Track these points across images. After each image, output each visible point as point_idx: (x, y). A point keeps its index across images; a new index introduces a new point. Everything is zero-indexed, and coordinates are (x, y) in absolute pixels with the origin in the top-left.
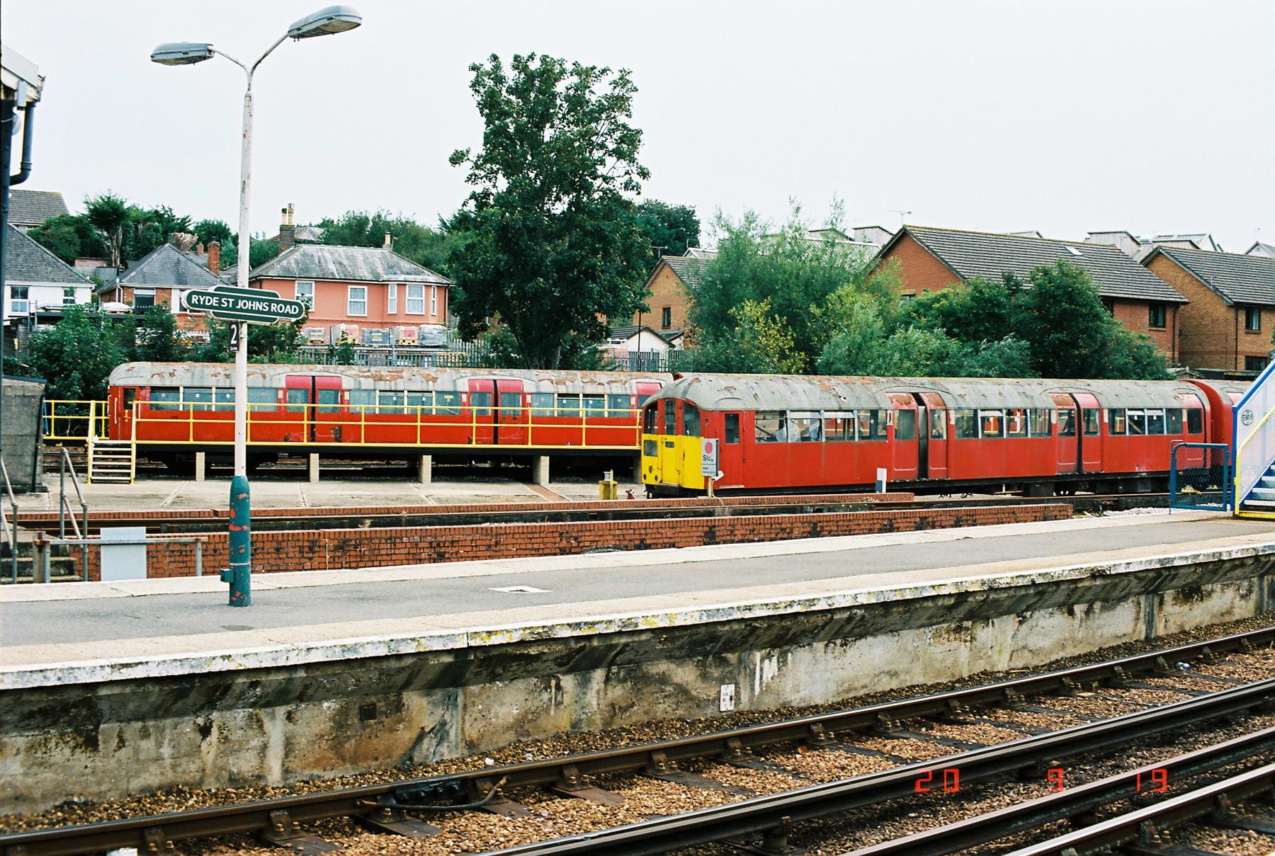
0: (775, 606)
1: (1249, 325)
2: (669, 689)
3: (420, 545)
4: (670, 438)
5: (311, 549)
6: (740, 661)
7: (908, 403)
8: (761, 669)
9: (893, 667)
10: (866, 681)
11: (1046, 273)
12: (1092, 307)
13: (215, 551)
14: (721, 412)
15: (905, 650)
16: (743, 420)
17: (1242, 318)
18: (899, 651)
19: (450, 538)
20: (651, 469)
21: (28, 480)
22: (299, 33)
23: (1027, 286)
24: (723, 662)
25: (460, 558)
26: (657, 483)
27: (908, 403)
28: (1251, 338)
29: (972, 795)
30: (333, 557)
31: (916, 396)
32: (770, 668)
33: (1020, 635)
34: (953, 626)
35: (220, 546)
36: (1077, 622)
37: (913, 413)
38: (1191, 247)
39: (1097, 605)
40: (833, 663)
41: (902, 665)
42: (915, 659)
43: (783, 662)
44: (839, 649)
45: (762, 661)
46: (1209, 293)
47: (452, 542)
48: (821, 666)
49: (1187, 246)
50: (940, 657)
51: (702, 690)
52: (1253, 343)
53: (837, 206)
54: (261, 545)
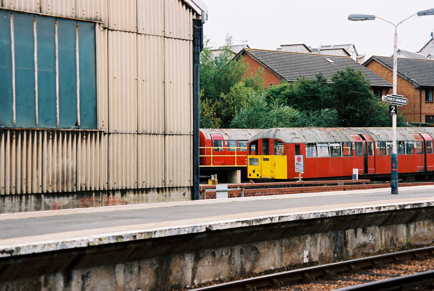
1: (427, 98)
4: (266, 157)
7: (359, 139)
11: (342, 74)
12: (367, 92)
14: (294, 144)
16: (301, 147)
17: (424, 95)
20: (254, 171)
22: (420, 14)
23: (329, 81)
26: (259, 177)
27: (359, 139)
28: (428, 105)
31: (361, 135)
37: (361, 143)
38: (344, 55)
46: (404, 81)
49: (341, 53)
52: (429, 108)
53: (229, 40)
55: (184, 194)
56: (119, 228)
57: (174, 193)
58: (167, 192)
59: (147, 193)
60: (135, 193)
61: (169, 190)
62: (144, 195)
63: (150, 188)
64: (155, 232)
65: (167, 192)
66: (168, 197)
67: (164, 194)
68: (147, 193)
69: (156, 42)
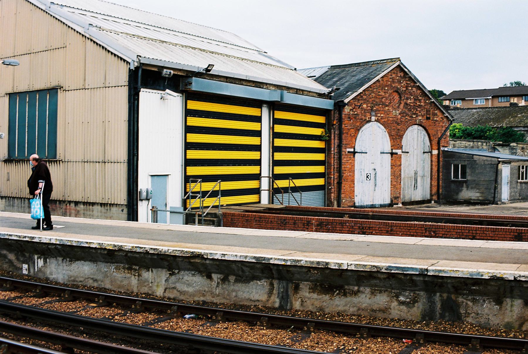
0: (20, 237)
2: (7, 260)
3: (355, 227)
5: (308, 225)
6: (30, 257)
8: (37, 262)
9: (95, 277)
10: (82, 279)
13: (271, 221)
15: (101, 271)
18: (97, 270)
19: (368, 226)
21: (492, 199)
24: (24, 256)
25: (372, 234)
29: (24, 319)
30: (317, 229)
32: (40, 263)
33: (170, 281)
34: (127, 266)
35: (273, 220)
36: (214, 284)
39: (232, 278)
40: (65, 268)
41: (99, 277)
42: (106, 276)
43: (45, 262)
44: (68, 263)
45: (38, 259)
47: (369, 227)
48: (61, 267)
50: (120, 279)
51: (16, 263)
54: (288, 221)
55: (122, 210)
56: (91, 237)
57: (114, 209)
58: (108, 207)
59: (93, 206)
60: (84, 205)
61: (110, 206)
62: (91, 207)
63: (114, 204)
64: (271, 258)
65: (108, 207)
66: (109, 211)
67: (106, 208)
68: (93, 206)
69: (90, 83)
